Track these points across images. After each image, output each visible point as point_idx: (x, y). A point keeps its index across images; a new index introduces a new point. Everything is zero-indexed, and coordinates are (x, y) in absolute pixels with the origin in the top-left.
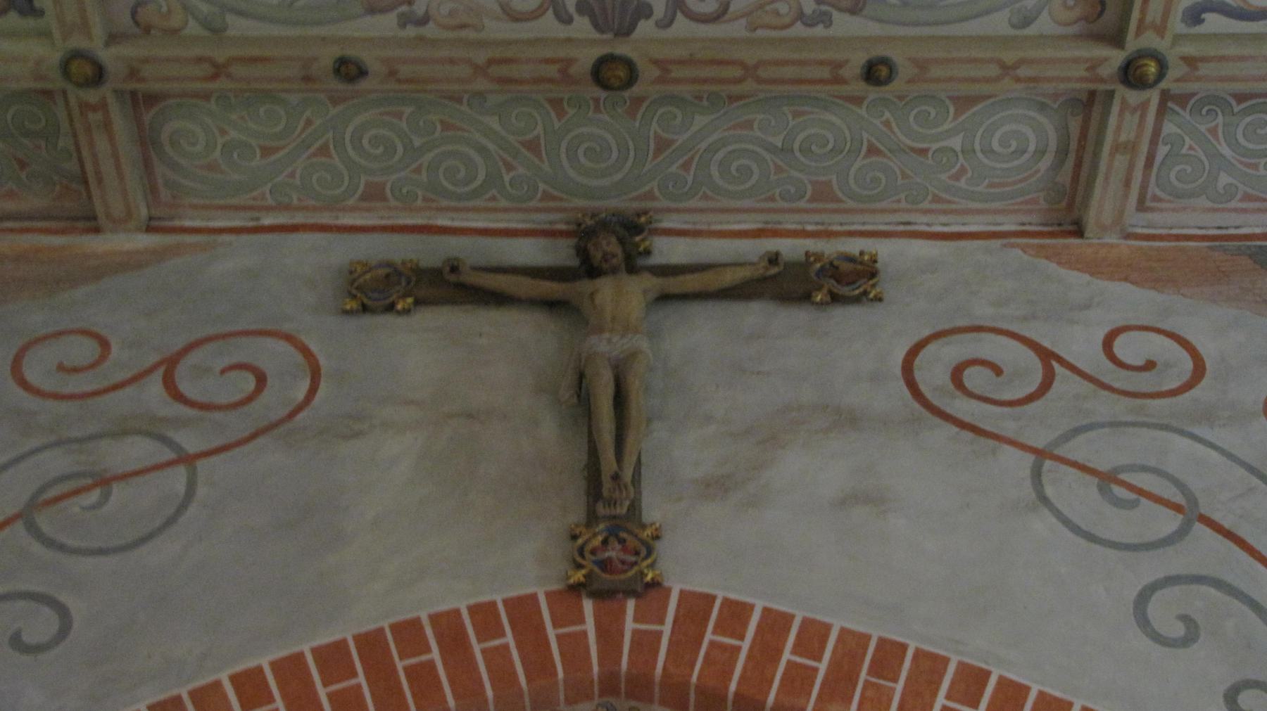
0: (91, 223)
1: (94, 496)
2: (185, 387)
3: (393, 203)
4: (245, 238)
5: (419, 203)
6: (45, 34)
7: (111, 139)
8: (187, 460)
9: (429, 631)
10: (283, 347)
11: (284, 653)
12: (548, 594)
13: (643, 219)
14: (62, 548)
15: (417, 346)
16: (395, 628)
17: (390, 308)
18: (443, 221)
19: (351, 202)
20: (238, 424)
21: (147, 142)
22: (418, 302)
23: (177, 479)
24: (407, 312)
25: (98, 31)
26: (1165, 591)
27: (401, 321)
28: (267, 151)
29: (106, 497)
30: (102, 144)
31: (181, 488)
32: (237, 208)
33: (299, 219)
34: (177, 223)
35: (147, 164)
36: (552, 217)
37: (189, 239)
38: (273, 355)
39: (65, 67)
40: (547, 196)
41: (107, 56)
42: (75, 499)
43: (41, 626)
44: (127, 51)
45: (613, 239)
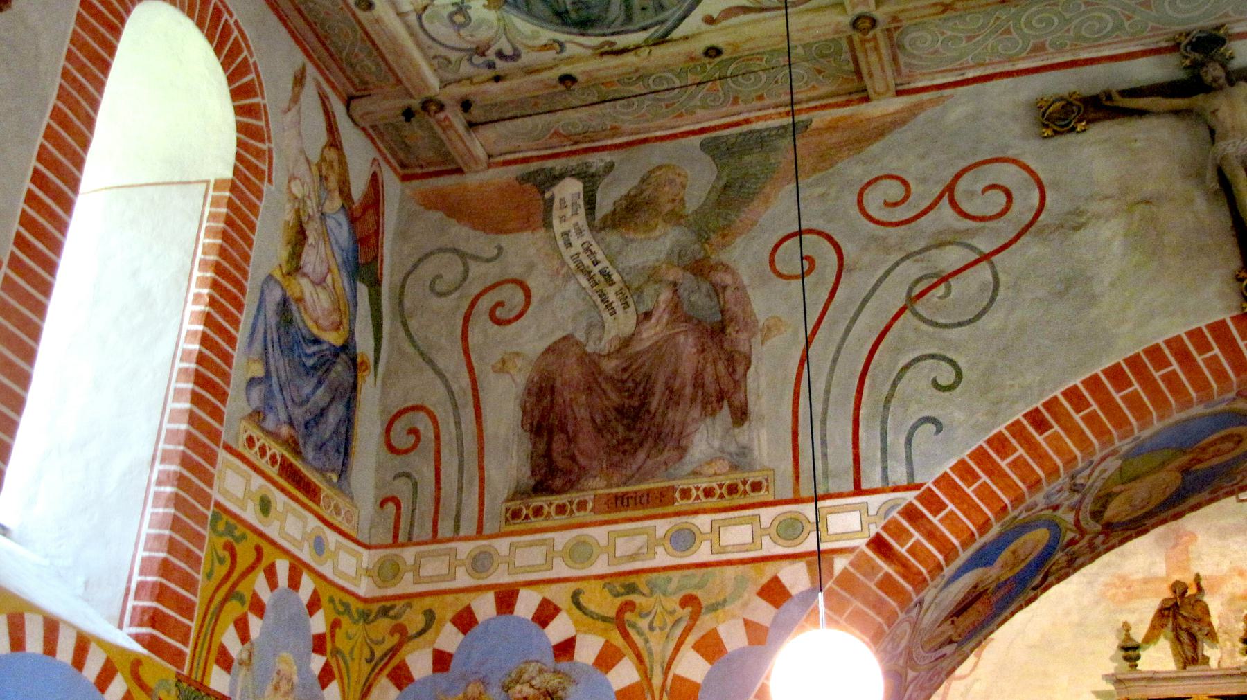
1: (941, 290)
2: (966, 207)
3: (1051, 50)
4: (960, 89)
5: (1068, 48)
7: (879, 55)
8: (986, 257)
9: (1167, 352)
10: (1012, 168)
11: (1088, 375)
12: (1232, 318)
13: (1222, 32)
14: (937, 325)
15: (1095, 154)
16: (1147, 352)
17: (1073, 129)
18: (1084, 55)
19: (1024, 55)
20: (1006, 228)
22: (1089, 122)
23: (984, 271)
24: (1083, 131)
27: (1081, 137)
28: (969, 39)
29: (949, 289)
30: (873, 58)
31: (990, 278)
32: (951, 70)
33: (990, 71)
34: (912, 86)
35: (895, 59)
36: (1157, 39)
38: (1008, 175)
39: (854, 24)
40: (1153, 29)
41: (879, 14)
42: (933, 292)
43: (947, 377)
45: (1218, 67)
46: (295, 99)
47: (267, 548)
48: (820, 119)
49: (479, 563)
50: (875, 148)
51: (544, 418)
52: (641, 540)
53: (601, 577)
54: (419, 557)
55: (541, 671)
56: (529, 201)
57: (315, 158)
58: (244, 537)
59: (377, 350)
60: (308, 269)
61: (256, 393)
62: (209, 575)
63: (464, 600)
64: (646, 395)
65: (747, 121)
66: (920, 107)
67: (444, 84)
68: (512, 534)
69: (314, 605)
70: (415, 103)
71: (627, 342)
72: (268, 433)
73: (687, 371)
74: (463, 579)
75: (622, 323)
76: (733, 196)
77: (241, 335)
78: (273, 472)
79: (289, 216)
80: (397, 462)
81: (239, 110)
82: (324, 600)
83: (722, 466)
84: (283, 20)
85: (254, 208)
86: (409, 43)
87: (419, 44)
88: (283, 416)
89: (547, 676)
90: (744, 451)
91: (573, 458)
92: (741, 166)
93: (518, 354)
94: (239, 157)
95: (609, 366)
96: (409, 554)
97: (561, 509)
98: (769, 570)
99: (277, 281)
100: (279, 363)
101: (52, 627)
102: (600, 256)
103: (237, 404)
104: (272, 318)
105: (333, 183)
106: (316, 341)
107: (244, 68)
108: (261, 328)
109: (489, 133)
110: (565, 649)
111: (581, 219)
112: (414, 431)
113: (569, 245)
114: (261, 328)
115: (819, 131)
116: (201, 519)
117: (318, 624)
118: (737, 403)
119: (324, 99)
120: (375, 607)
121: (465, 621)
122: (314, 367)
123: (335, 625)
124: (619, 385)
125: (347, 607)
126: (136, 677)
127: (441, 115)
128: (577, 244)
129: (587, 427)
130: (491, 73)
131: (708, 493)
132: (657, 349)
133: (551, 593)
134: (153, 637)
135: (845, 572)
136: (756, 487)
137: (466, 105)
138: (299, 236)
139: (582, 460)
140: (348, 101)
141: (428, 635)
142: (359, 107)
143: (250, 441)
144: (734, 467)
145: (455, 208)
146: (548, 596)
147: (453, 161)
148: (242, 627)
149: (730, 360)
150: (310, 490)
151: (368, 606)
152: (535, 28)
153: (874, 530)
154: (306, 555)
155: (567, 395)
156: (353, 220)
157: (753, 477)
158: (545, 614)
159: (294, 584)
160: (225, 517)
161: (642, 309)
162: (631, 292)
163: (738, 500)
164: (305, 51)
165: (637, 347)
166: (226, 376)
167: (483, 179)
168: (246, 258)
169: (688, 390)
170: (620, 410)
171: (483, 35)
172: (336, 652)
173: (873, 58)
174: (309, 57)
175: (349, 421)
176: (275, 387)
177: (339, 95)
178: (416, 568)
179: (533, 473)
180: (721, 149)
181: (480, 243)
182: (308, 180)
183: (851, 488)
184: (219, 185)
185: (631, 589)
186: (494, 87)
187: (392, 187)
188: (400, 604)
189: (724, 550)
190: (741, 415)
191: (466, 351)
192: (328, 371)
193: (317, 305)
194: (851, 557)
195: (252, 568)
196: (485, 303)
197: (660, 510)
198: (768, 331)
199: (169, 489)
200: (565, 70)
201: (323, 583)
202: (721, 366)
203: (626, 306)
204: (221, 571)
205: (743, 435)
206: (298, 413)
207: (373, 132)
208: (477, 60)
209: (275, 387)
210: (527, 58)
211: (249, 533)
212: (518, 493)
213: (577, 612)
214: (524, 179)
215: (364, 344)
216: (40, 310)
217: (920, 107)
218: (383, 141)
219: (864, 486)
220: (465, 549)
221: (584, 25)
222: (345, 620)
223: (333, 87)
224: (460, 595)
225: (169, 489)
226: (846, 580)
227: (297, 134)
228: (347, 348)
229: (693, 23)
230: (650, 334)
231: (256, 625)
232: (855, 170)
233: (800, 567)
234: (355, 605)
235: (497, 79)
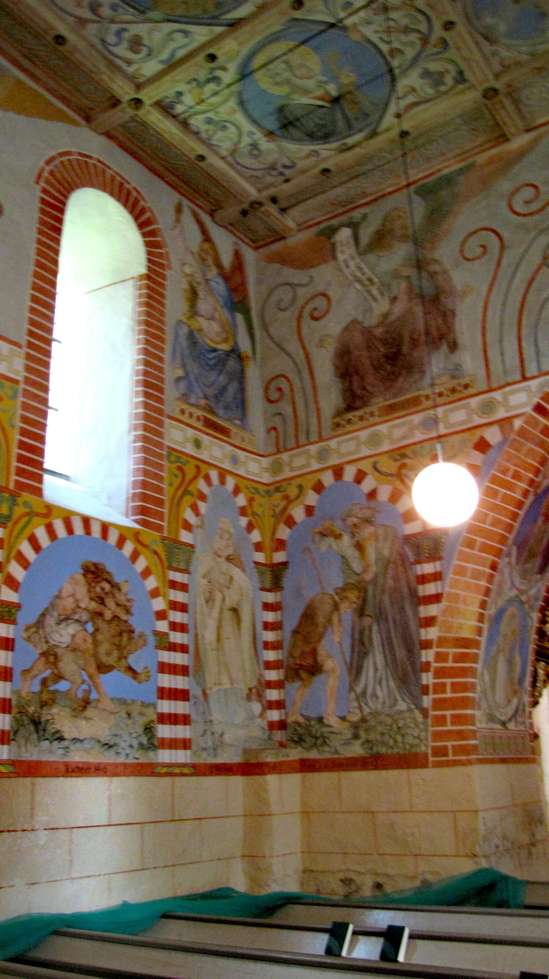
0: (505, 138)
6: (473, 87)
21: (516, 102)
25: (491, 77)
26: (387, 471)
35: (520, 111)
37: (543, 129)
39: (485, 97)
41: (497, 85)
44: (505, 79)
46: (178, 220)
47: (202, 466)
48: (481, 159)
49: (322, 455)
50: (516, 169)
51: (347, 369)
52: (405, 429)
53: (386, 452)
54: (291, 456)
55: (361, 509)
56: (322, 248)
57: (196, 249)
58: (187, 462)
59: (254, 349)
60: (202, 312)
61: (182, 385)
62: (171, 485)
63: (317, 476)
64: (399, 346)
65: (439, 170)
66: (540, 137)
67: (259, 191)
68: (336, 436)
69: (236, 491)
70: (246, 206)
71: (386, 316)
72: (193, 405)
73: (420, 326)
74: (315, 465)
75: (382, 306)
76: (437, 216)
77: (167, 356)
78: (199, 425)
79: (185, 286)
80: (272, 408)
81: (144, 235)
82: (243, 489)
83: (446, 378)
84: (163, 178)
85: (162, 286)
86: (232, 173)
87: (239, 173)
88: (201, 395)
89: (364, 511)
90: (458, 367)
91: (364, 389)
92: (440, 199)
93: (327, 335)
94: (149, 261)
95: (378, 332)
96: (285, 457)
97: (361, 418)
98: (478, 434)
99: (184, 323)
100: (194, 368)
101: (86, 521)
102: (366, 270)
103: (171, 393)
104: (184, 343)
105: (210, 260)
106: (215, 350)
107: (143, 211)
108: (178, 350)
109: (294, 212)
110: (372, 494)
111: (352, 250)
112: (280, 389)
113: (347, 266)
114: (178, 350)
115: (482, 166)
116: (160, 456)
117: (241, 500)
118: (450, 340)
119: (196, 216)
120: (272, 488)
121: (319, 488)
122: (215, 365)
123: (251, 500)
124: (384, 342)
125: (257, 490)
126: (138, 541)
127: (262, 209)
128: (351, 264)
129: (371, 371)
130: (282, 178)
131: (440, 395)
132: (402, 319)
133: (362, 465)
134: (143, 519)
135: (522, 429)
136: (466, 386)
137: (274, 200)
138: (193, 295)
139: (369, 388)
140: (212, 214)
141: (301, 498)
142: (219, 215)
143: (183, 412)
144: (453, 377)
145: (284, 259)
146: (360, 468)
147: (278, 233)
148: (195, 509)
149: (444, 315)
150: (224, 431)
151: (269, 488)
152: (299, 146)
153: (536, 400)
154: (227, 466)
155: (357, 353)
156: (227, 279)
157: (464, 381)
158: (360, 477)
159: (222, 481)
160: (175, 453)
161: (392, 295)
162: (385, 287)
163: (458, 396)
164: (180, 193)
165: (392, 318)
166: (161, 380)
167: (297, 239)
168: (162, 313)
169: (423, 338)
170: (386, 356)
171: (271, 158)
172: (254, 514)
173: (503, 113)
174: (183, 195)
175: (242, 390)
176: (193, 381)
177: (207, 212)
178: (290, 464)
179: (345, 400)
180: (426, 191)
181: (298, 276)
182: (193, 263)
183: (518, 377)
184: (141, 277)
185: (404, 456)
186: (286, 186)
187: (250, 256)
188: (284, 484)
189: (452, 426)
190: (454, 346)
191: (301, 339)
192: (224, 365)
193: (211, 330)
194: (523, 418)
195: (195, 477)
196: (308, 309)
197: (415, 409)
198: (464, 294)
199: (139, 444)
200: (323, 166)
201: (239, 478)
202: (440, 320)
203: (382, 294)
204: (177, 481)
205: (456, 358)
206: (210, 392)
207: (229, 226)
208: (274, 173)
209: (193, 381)
210: (300, 165)
211: (190, 459)
212: (339, 413)
213: (376, 474)
214: (321, 233)
215: (245, 346)
216: (47, 365)
217: (540, 137)
218: (238, 230)
219: (528, 375)
220: (313, 449)
221: (326, 137)
222: (257, 497)
223: (200, 207)
224: (314, 474)
225: (139, 444)
226: (522, 433)
227: (183, 240)
228: (235, 352)
229: (389, 120)
230: (398, 309)
231: (203, 507)
232: (505, 186)
233: (495, 429)
234: (262, 488)
235: (287, 181)
